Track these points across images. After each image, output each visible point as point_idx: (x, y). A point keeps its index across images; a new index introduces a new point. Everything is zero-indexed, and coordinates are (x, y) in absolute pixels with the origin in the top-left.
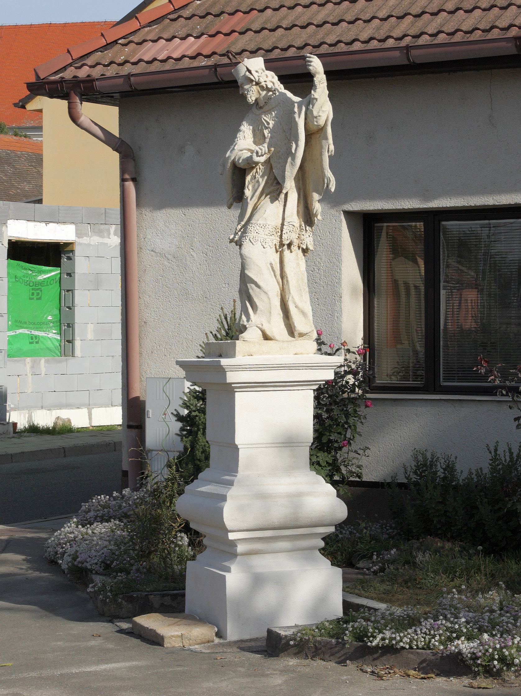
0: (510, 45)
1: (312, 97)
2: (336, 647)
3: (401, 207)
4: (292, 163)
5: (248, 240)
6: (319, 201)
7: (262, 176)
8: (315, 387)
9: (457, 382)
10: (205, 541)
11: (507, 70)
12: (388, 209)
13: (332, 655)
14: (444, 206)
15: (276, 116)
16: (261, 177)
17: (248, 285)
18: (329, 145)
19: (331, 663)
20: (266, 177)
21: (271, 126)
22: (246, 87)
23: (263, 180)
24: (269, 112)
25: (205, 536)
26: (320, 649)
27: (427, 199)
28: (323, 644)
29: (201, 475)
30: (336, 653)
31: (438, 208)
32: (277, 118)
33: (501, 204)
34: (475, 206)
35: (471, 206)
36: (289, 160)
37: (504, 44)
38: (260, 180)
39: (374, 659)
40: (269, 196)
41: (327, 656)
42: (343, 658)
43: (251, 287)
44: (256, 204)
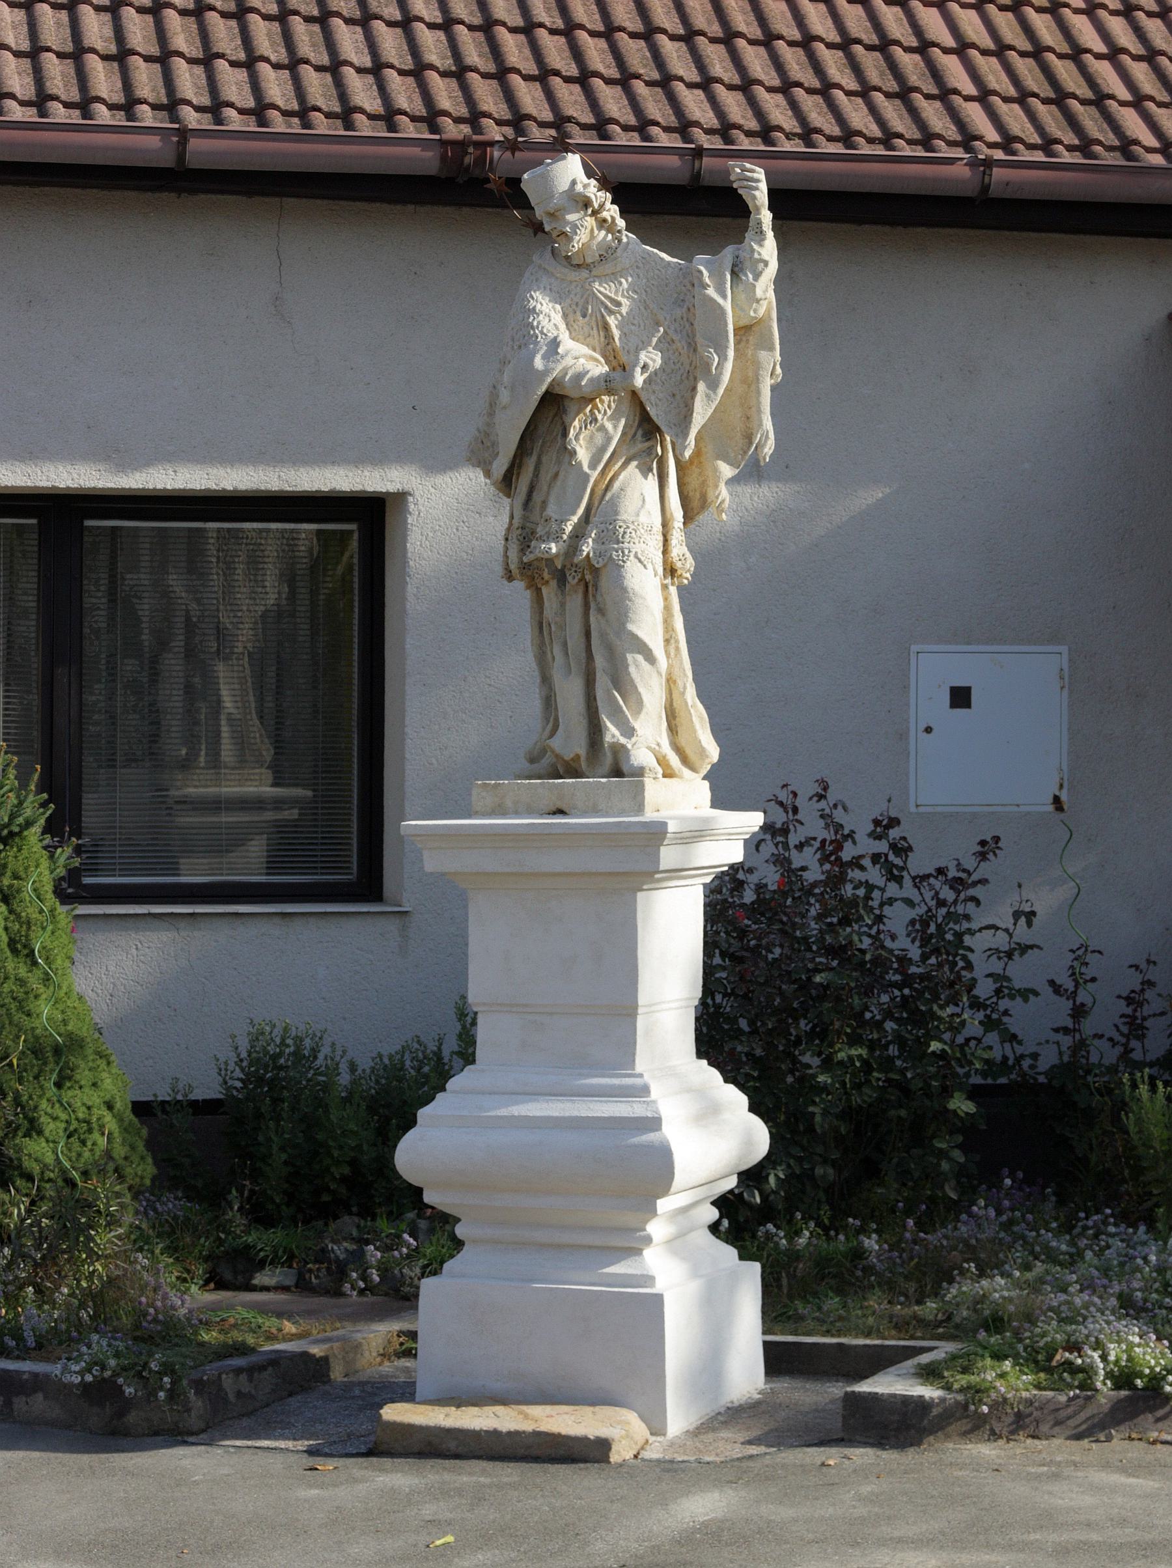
0: (430, 154)
1: (756, 256)
2: (1068, 1406)
3: (49, 484)
4: (707, 396)
5: (632, 557)
6: (730, 482)
7: (614, 418)
8: (708, 879)
9: (120, 876)
10: (460, 1231)
11: (319, 202)
12: (13, 487)
13: (1058, 1423)
14: (159, 487)
15: (632, 288)
16: (611, 419)
17: (629, 657)
18: (771, 361)
19: (1056, 1442)
20: (623, 421)
21: (624, 310)
22: (571, 217)
23: (615, 427)
24: (613, 277)
25: (459, 1220)
26: (1030, 1414)
27: (123, 465)
28: (1036, 1404)
29: (450, 1085)
30: (1069, 1418)
31: (143, 489)
32: (635, 292)
33: (299, 489)
34: (235, 491)
35: (224, 490)
36: (701, 387)
37: (416, 151)
38: (609, 426)
39: (1158, 1420)
40: (634, 463)
41: (1044, 1428)
42: (1084, 1427)
43: (635, 660)
44: (532, 481)
